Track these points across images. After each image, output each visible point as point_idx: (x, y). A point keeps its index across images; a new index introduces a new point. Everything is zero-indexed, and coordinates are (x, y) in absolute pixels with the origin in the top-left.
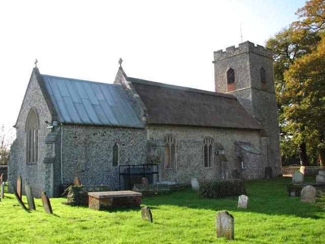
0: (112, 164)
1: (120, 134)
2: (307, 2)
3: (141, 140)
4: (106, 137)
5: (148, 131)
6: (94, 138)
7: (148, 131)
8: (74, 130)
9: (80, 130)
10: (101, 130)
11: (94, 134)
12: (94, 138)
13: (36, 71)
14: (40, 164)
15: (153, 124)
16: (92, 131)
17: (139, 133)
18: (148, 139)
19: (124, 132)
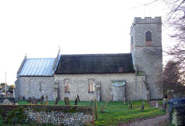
0: (39, 90)
1: (42, 78)
2: (130, 34)
3: (52, 81)
4: (37, 80)
5: (56, 77)
6: (32, 81)
7: (56, 77)
8: (25, 78)
9: (26, 78)
10: (34, 78)
11: (32, 79)
12: (32, 81)
13: (26, 57)
14: (136, 71)
15: (160, 100)
16: (31, 78)
17: (51, 78)
18: (56, 80)
19: (44, 78)
